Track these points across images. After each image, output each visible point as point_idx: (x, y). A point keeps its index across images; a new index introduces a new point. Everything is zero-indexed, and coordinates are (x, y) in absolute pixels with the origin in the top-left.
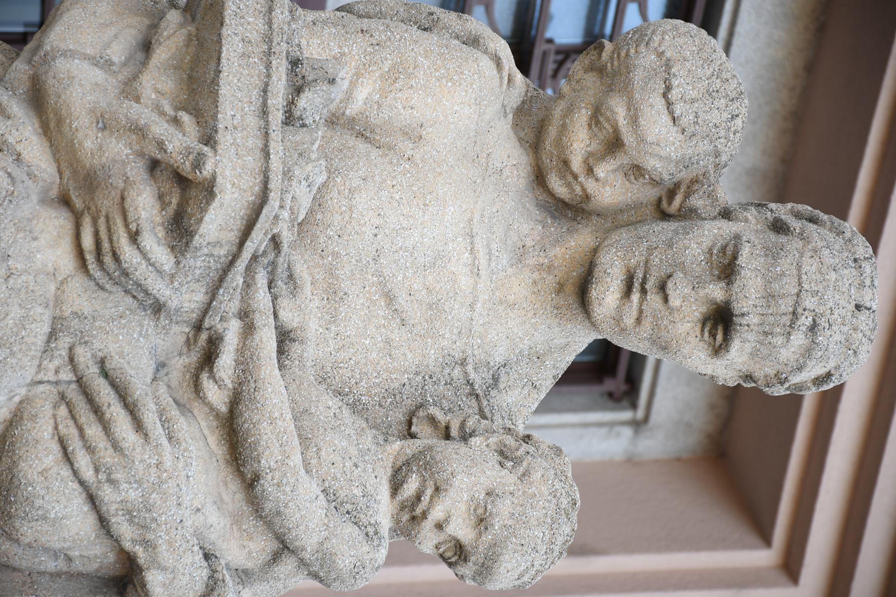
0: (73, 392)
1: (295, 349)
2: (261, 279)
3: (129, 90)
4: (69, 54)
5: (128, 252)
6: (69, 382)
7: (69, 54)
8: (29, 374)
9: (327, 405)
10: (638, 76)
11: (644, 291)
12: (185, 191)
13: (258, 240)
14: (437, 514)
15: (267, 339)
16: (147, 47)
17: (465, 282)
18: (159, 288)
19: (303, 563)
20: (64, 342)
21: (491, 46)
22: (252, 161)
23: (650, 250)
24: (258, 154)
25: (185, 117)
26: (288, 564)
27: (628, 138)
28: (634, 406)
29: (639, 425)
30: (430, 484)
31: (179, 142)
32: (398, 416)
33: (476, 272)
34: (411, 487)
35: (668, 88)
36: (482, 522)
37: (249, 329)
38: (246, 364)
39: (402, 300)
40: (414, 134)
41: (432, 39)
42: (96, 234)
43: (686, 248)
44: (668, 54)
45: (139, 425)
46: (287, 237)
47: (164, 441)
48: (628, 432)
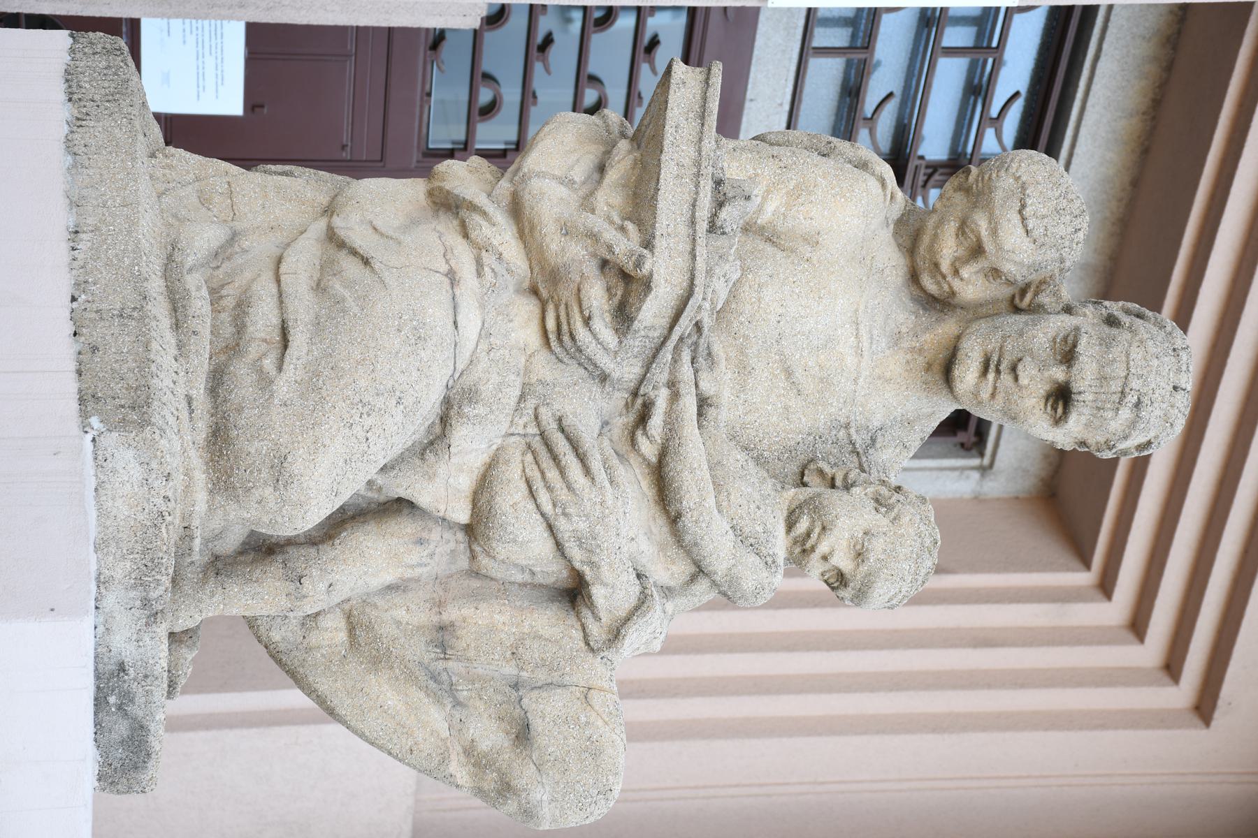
0: (537, 443)
1: (711, 412)
2: (686, 356)
5: (582, 333)
6: (535, 435)
10: (998, 196)
11: (998, 372)
14: (823, 548)
15: (689, 404)
16: (601, 169)
17: (850, 360)
18: (605, 362)
19: (714, 584)
20: (531, 403)
22: (682, 262)
23: (1004, 338)
24: (687, 256)
25: (630, 226)
26: (702, 585)
27: (989, 246)
28: (982, 455)
29: (984, 470)
31: (624, 245)
34: (803, 526)
35: (1023, 206)
37: (675, 396)
39: (799, 374)
40: (812, 240)
42: (558, 318)
43: (1034, 337)
44: (1024, 178)
45: (587, 471)
48: (976, 475)
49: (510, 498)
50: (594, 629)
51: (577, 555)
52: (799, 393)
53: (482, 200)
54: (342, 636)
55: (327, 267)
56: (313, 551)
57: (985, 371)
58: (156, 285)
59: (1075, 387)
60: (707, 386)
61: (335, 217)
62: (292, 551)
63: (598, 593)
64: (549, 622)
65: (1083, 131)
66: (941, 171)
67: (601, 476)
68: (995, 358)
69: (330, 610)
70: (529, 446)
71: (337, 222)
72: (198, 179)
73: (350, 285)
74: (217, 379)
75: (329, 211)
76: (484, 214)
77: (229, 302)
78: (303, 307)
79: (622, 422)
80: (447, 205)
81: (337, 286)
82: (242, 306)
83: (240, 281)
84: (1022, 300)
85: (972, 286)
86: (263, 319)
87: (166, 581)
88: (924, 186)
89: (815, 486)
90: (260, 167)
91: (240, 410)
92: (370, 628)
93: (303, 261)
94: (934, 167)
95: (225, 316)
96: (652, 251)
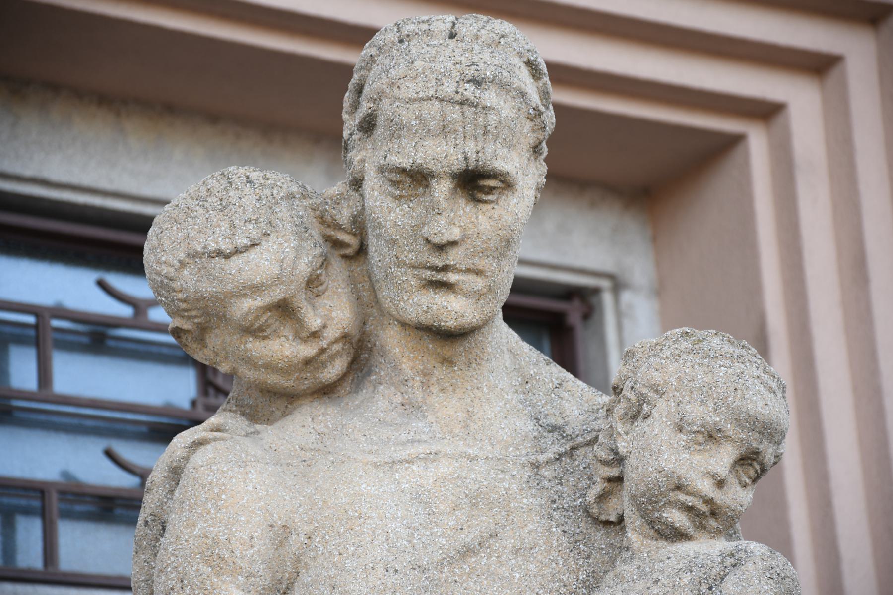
11: (445, 268)
14: (706, 487)
17: (444, 468)
27: (276, 294)
28: (596, 291)
29: (618, 285)
33: (433, 457)
34: (677, 518)
35: (220, 253)
36: (712, 436)
39: (468, 537)
40: (282, 533)
48: (626, 297)
52: (494, 535)
59: (458, 165)
85: (333, 313)
89: (621, 504)
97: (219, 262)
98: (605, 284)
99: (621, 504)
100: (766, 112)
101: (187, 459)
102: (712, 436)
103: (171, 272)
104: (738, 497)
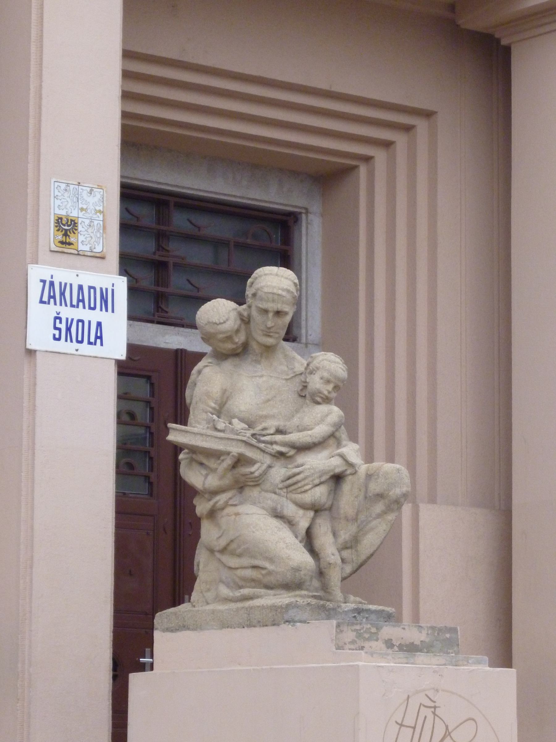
1: (281, 428)
2: (263, 439)
3: (214, 471)
4: (204, 484)
5: (257, 474)
7: (204, 484)
8: (285, 499)
9: (296, 421)
10: (212, 331)
11: (270, 332)
12: (240, 461)
13: (254, 442)
14: (326, 393)
15: (279, 438)
16: (201, 464)
17: (264, 379)
18: (264, 467)
19: (337, 430)
20: (277, 491)
21: (201, 367)
25: (222, 458)
26: (337, 434)
27: (229, 334)
28: (300, 213)
29: (307, 212)
30: (318, 394)
31: (228, 462)
32: (301, 400)
33: (262, 376)
34: (319, 399)
35: (216, 323)
36: (328, 382)
37: (276, 443)
38: (284, 444)
39: (269, 397)
40: (224, 391)
41: (199, 384)
42: (251, 482)
45: (298, 474)
46: (252, 431)
47: (303, 467)
48: (311, 217)
49: (307, 498)
50: (348, 472)
51: (324, 479)
52: (275, 397)
53: (211, 503)
54: (349, 551)
55: (233, 554)
56: (321, 560)
57: (269, 336)
58: (240, 605)
59: (276, 309)
60: (272, 431)
61: (215, 549)
62: (322, 566)
63: (338, 470)
64: (346, 487)
65: (146, 178)
66: (161, 243)
67: (300, 469)
68: (265, 333)
69: (340, 555)
70: (291, 492)
71: (217, 548)
72: (202, 592)
73: (239, 547)
74: (268, 587)
75: (211, 551)
76: (216, 503)
77: (243, 583)
78: (246, 561)
79: (283, 461)
80: (212, 514)
81: (239, 551)
82: (244, 579)
83: (237, 580)
84: (246, 321)
85: (241, 338)
86: (249, 573)
87: (328, 603)
88: (168, 251)
89: (306, 392)
90: (195, 572)
91: (278, 581)
92: (346, 542)
93: (233, 562)
94: (159, 247)
95: (248, 585)
96: (231, 452)
97: (216, 325)
98: (304, 211)
99: (306, 392)
100: (368, 159)
101: (203, 369)
102: (328, 382)
103: (203, 325)
104: (334, 395)
